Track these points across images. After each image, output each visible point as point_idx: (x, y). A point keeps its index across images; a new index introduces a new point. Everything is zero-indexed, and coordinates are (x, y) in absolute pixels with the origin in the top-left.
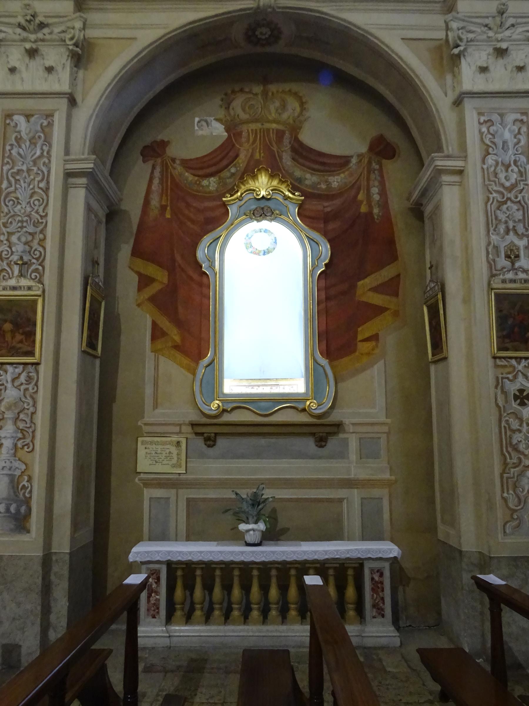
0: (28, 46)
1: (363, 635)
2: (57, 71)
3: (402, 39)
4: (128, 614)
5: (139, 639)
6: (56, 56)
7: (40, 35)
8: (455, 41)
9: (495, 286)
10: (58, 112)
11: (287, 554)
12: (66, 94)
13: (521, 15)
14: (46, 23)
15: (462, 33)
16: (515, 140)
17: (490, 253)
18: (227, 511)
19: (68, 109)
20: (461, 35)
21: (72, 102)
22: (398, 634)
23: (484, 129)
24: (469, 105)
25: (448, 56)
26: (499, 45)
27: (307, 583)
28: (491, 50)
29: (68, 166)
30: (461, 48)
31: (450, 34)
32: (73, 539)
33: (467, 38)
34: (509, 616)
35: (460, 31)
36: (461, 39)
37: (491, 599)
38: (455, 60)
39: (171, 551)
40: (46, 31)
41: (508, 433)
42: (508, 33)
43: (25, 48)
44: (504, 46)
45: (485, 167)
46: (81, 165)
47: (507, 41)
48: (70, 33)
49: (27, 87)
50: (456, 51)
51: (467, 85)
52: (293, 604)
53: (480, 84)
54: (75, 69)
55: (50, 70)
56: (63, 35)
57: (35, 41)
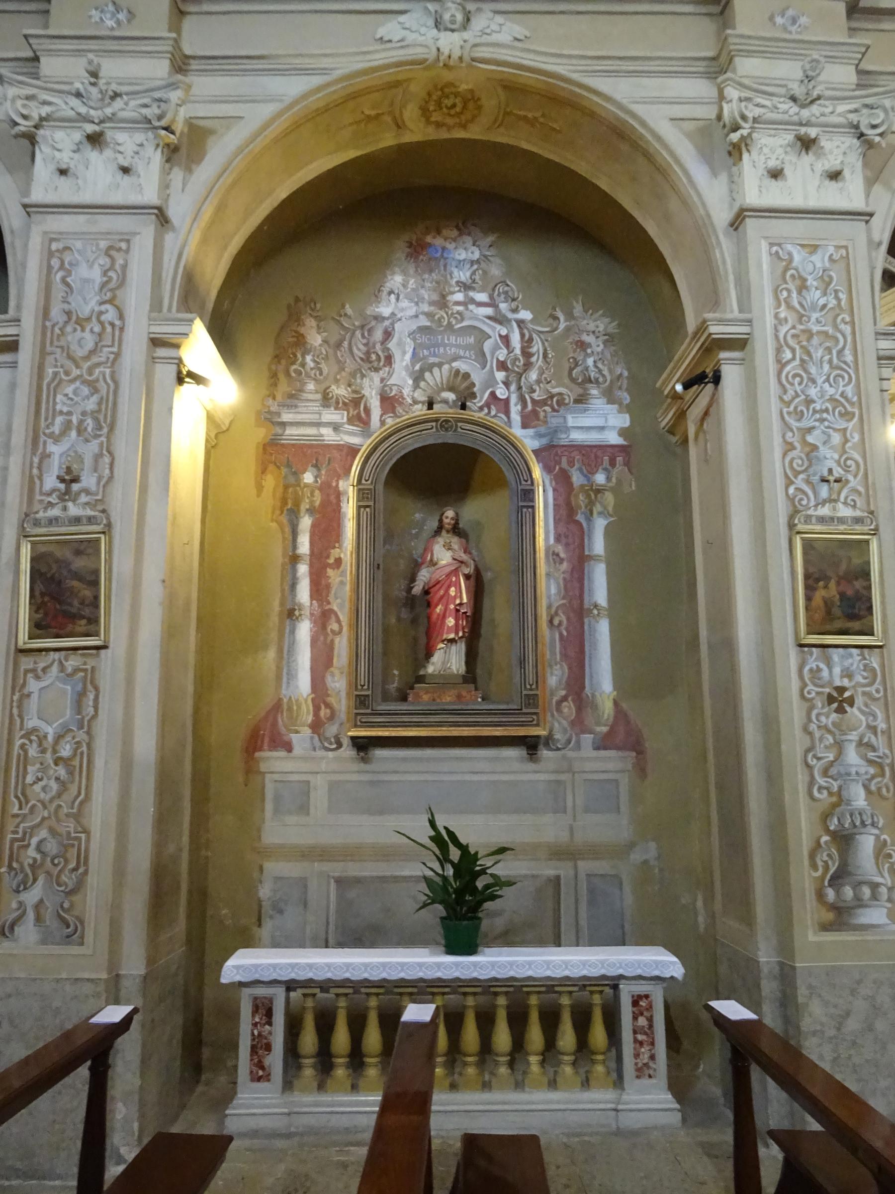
0: (90, 128)
1: (620, 1107)
3: (672, 119)
4: (92, 1063)
5: (432, 1115)
7: (108, 111)
8: (734, 119)
9: (800, 527)
10: (138, 237)
11: (281, 969)
14: (118, 92)
15: (746, 107)
16: (105, 279)
17: (107, 466)
19: (156, 230)
20: (744, 110)
22: (677, 1106)
23: (55, 263)
24: (751, 225)
25: (727, 144)
26: (803, 130)
28: (790, 137)
29: (154, 329)
30: (745, 132)
31: (726, 106)
33: (40, 115)
35: (743, 104)
36: (744, 118)
38: (736, 151)
39: (260, 965)
40: (118, 103)
41: (76, 762)
45: (48, 324)
46: (166, 327)
49: (797, 201)
50: (735, 137)
52: (568, 1055)
53: (65, 192)
54: (167, 166)
57: (102, 122)
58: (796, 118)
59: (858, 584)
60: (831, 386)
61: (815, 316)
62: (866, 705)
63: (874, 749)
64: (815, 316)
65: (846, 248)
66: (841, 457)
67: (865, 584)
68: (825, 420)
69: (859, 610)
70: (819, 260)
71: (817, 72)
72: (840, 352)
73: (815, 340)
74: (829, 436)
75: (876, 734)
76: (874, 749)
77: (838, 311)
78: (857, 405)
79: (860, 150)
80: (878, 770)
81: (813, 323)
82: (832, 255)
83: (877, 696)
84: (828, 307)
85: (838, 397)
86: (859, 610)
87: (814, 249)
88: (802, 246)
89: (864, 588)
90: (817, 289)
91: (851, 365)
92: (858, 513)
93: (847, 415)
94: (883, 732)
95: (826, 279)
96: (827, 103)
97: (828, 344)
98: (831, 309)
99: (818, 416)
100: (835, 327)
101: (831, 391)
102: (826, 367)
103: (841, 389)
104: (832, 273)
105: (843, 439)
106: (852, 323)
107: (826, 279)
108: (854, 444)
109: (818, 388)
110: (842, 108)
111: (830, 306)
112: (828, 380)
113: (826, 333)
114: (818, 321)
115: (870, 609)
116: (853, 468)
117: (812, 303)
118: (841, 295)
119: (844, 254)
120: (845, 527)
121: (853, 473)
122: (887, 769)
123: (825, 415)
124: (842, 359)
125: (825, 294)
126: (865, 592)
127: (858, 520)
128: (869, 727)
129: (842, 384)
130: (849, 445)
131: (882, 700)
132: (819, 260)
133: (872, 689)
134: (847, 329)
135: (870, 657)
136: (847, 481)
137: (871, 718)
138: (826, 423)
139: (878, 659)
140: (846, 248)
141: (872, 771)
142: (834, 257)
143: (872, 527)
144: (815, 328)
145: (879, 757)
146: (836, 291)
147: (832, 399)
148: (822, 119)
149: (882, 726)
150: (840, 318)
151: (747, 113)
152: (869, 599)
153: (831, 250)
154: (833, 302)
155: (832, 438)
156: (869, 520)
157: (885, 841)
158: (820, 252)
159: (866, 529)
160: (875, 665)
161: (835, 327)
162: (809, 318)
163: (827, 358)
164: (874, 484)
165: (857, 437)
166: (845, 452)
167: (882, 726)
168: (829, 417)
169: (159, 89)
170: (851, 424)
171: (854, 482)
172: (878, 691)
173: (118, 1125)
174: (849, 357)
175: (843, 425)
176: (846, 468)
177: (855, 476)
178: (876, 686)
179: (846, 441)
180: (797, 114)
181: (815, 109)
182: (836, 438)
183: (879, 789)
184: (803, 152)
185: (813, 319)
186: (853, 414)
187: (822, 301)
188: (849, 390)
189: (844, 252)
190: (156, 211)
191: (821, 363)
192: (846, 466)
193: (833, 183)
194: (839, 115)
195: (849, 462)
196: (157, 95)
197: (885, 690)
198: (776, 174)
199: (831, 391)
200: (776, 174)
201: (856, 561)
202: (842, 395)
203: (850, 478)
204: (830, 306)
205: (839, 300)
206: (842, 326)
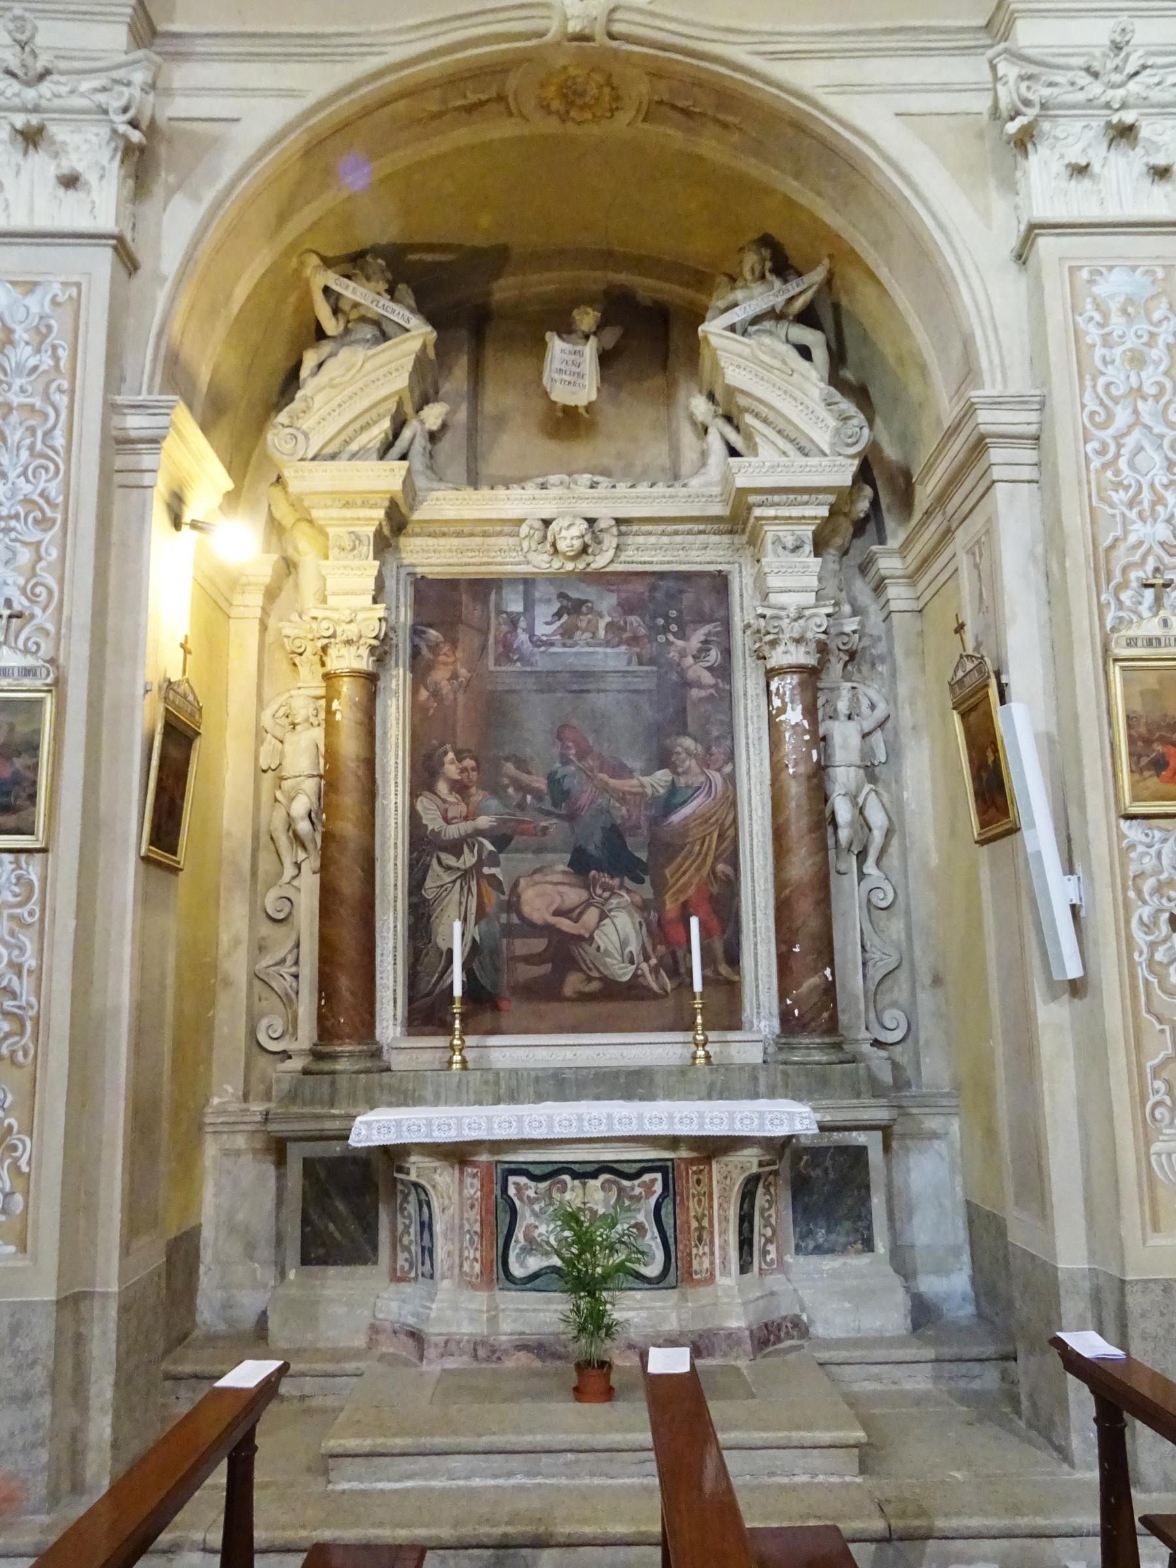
0: (20, 120)
2: (86, 183)
6: (89, 149)
12: (112, 237)
13: (1163, 49)
18: (295, 665)
21: (127, 259)
24: (1045, 244)
27: (750, 1523)
28: (1098, 124)
32: (123, 1276)
34: (1146, 1446)
37: (1101, 1403)
42: (1133, 86)
43: (13, 127)
44: (1129, 117)
47: (1135, 107)
48: (121, 94)
51: (1043, 211)
53: (1080, 202)
55: (70, 181)
56: (102, 98)
58: (17, 101)
59: (19, 763)
60: (28, 481)
61: (18, 382)
62: (12, 934)
63: (14, 996)
64: (18, 382)
65: (78, 285)
66: (27, 582)
67: (30, 762)
68: (13, 529)
69: (16, 798)
70: (36, 303)
71: (28, 34)
72: (47, 434)
73: (15, 417)
74: (14, 553)
75: (20, 976)
76: (14, 996)
77: (53, 375)
78: (61, 508)
79: (113, 145)
80: (16, 1027)
81: (16, 394)
82: (55, 296)
83: (29, 920)
84: (41, 369)
85: (35, 497)
86: (16, 798)
87: (30, 287)
88: (14, 283)
89: (28, 767)
90: (27, 343)
91: (61, 450)
92: (29, 661)
93: (44, 523)
94: (30, 972)
95: (44, 330)
96: (63, 79)
97: (32, 422)
98: (44, 372)
99: (1146, 496)
100: (46, 396)
101: (25, 488)
102: (24, 455)
103: (41, 486)
104: (53, 322)
105: (34, 557)
106: (72, 392)
107: (44, 330)
108: (50, 564)
109: (9, 485)
110: (86, 85)
111: (43, 367)
112: (24, 473)
113: (32, 407)
114: (22, 390)
115: (33, 797)
116: (43, 597)
117: (18, 365)
118: (60, 352)
119: (75, 294)
120: (9, 680)
121: (43, 604)
122: (29, 1026)
123: (13, 523)
124: (50, 443)
125: (38, 351)
126: (30, 775)
127: (28, 672)
128: (11, 964)
129: (44, 477)
130: (43, 564)
131: (37, 926)
132: (36, 303)
133: (24, 911)
134: (62, 400)
135: (27, 864)
136: (32, 616)
137: (16, 952)
138: (13, 535)
139: (39, 869)
140: (78, 285)
141: (6, 1027)
142: (60, 299)
143: (49, 681)
144: (16, 400)
145: (20, 1007)
146: (54, 348)
147: (27, 501)
148: (57, 102)
149: (30, 962)
150: (53, 386)
151: (1030, 96)
152: (34, 783)
153: (56, 288)
154: (47, 362)
155: (19, 557)
156: (44, 671)
157: (10, 1127)
158: (39, 291)
159: (38, 683)
160: (34, 878)
161: (46, 396)
162: (10, 386)
163: (28, 441)
164: (70, 619)
165: (55, 553)
166: (34, 574)
167: (30, 962)
168: (18, 527)
169: (119, 67)
170: (48, 536)
171: (43, 618)
172: (31, 914)
173: (633, 1529)
174: (59, 441)
175: (35, 535)
176: (33, 598)
177: (44, 610)
178: (30, 906)
179: (39, 558)
180: (17, 95)
181: (46, 88)
182: (25, 556)
183: (13, 1053)
184: (31, 147)
185: (16, 387)
186: (54, 521)
187: (32, 362)
188: (53, 488)
189: (74, 291)
190: (114, 242)
191: (18, 449)
192: (33, 594)
193: (71, 192)
194: (82, 95)
195: (38, 590)
196: (116, 74)
197: (43, 910)
198: (1080, 171)
199: (25, 488)
200: (1080, 171)
201: (22, 729)
202: (42, 495)
203: (37, 611)
204: (43, 367)
205: (57, 359)
206: (56, 397)
